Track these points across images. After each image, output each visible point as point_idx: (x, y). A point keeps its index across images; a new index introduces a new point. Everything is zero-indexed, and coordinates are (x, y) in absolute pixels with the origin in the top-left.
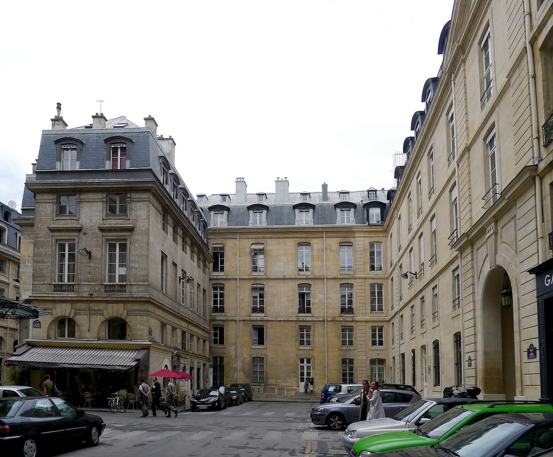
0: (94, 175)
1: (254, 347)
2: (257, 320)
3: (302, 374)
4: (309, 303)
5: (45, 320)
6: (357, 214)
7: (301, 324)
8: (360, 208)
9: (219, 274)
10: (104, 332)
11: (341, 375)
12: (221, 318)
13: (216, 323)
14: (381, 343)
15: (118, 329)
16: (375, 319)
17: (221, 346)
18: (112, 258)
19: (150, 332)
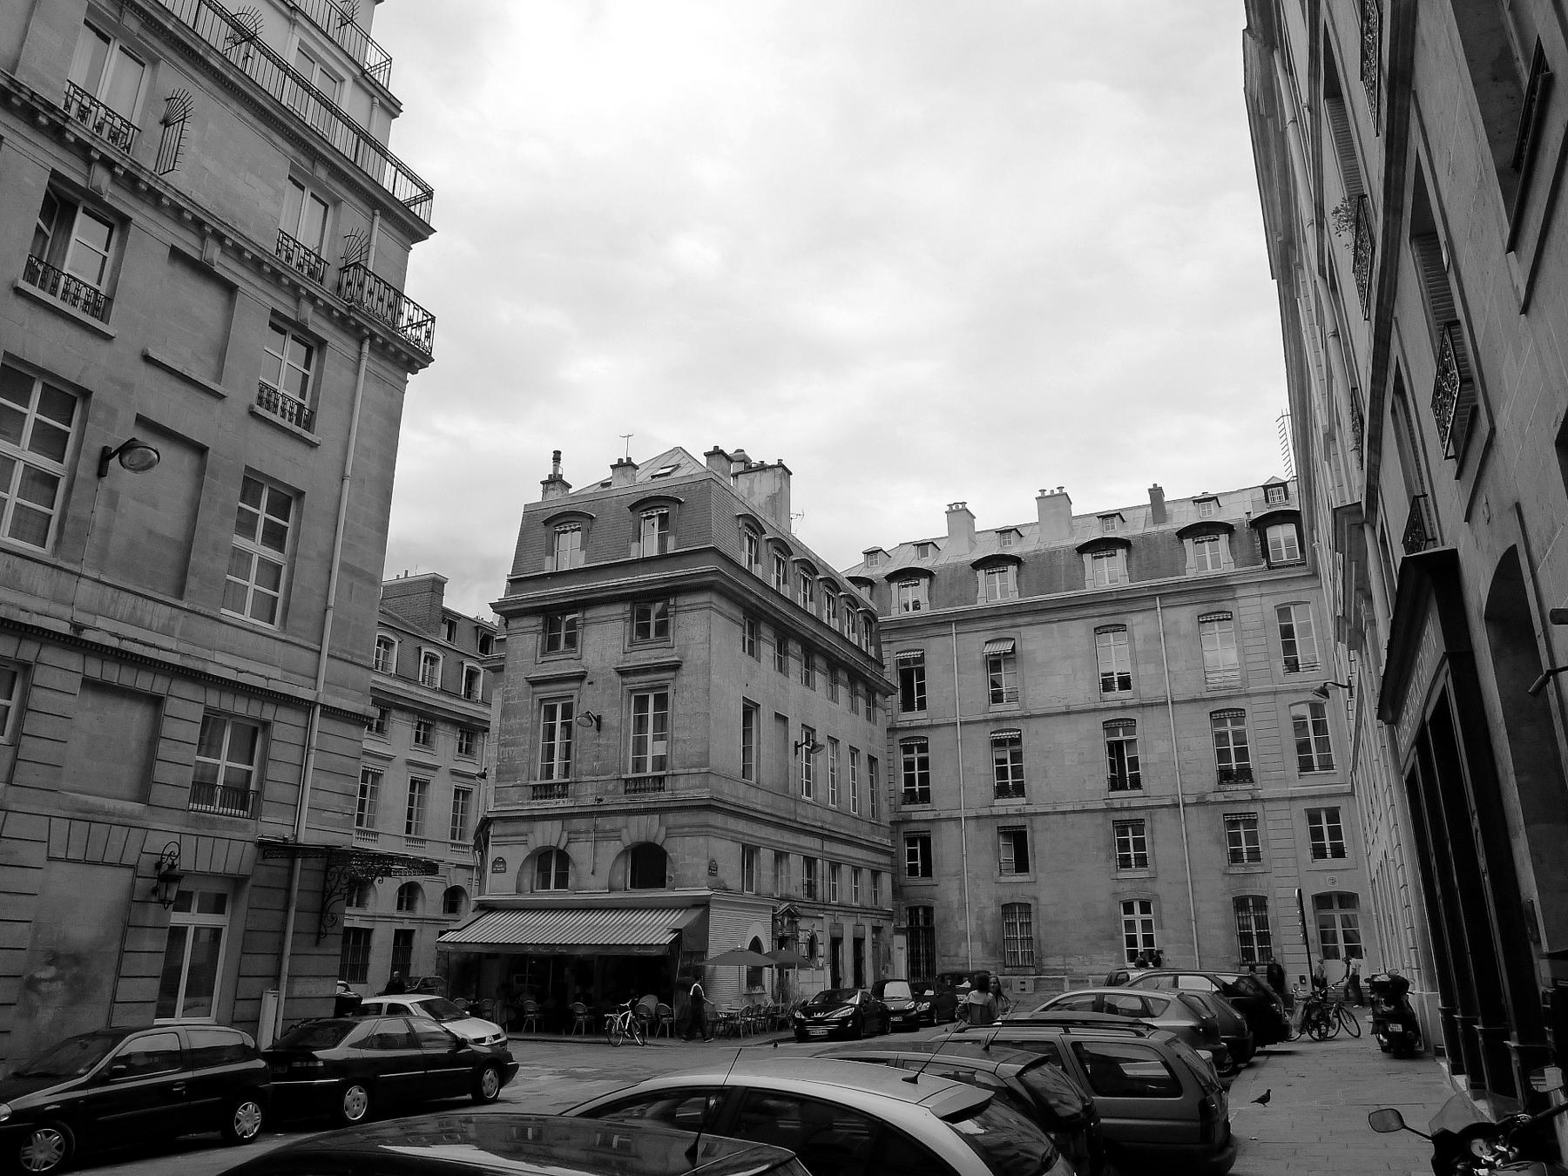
0: (610, 572)
1: (1003, 879)
2: (1007, 815)
3: (1132, 941)
4: (1134, 763)
5: (515, 856)
6: (1236, 544)
7: (1118, 816)
8: (1243, 532)
9: (917, 717)
10: (624, 873)
11: (1236, 940)
12: (923, 816)
13: (913, 827)
14: (1339, 852)
15: (648, 865)
16: (1314, 790)
17: (926, 881)
18: (641, 723)
19: (713, 869)
